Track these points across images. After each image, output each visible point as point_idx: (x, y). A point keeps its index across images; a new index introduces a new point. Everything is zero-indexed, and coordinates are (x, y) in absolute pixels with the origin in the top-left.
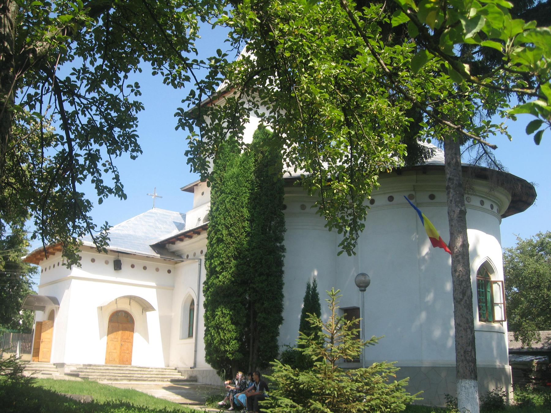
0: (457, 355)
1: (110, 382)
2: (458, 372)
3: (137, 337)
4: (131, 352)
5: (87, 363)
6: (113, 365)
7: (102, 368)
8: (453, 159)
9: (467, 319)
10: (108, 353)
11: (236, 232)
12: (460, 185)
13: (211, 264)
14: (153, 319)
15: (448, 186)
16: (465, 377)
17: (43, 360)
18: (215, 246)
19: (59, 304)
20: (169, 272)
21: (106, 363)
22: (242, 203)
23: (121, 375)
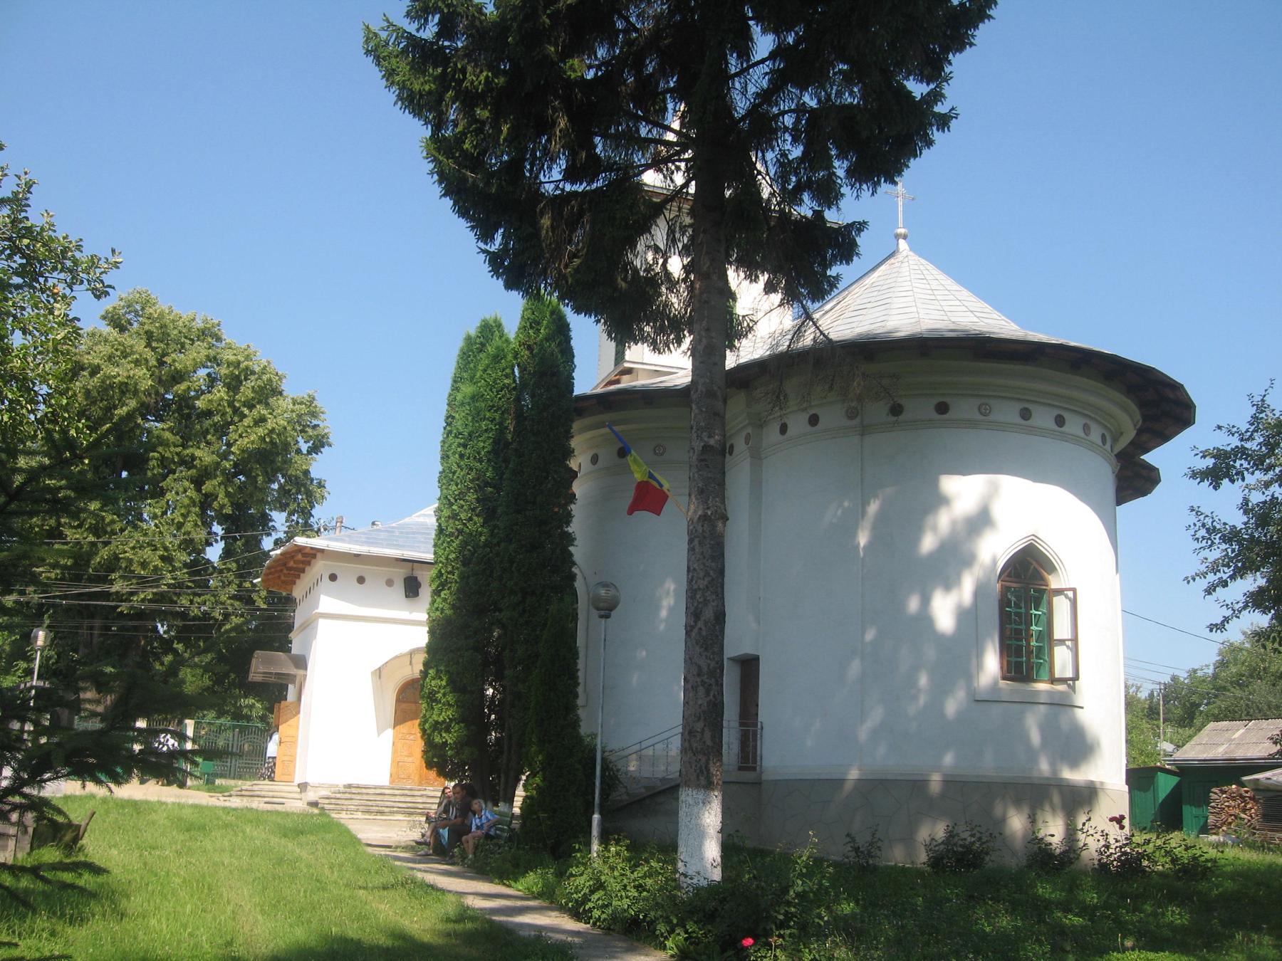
5: (346, 783)
9: (699, 667)
10: (396, 763)
17: (284, 778)
21: (392, 782)
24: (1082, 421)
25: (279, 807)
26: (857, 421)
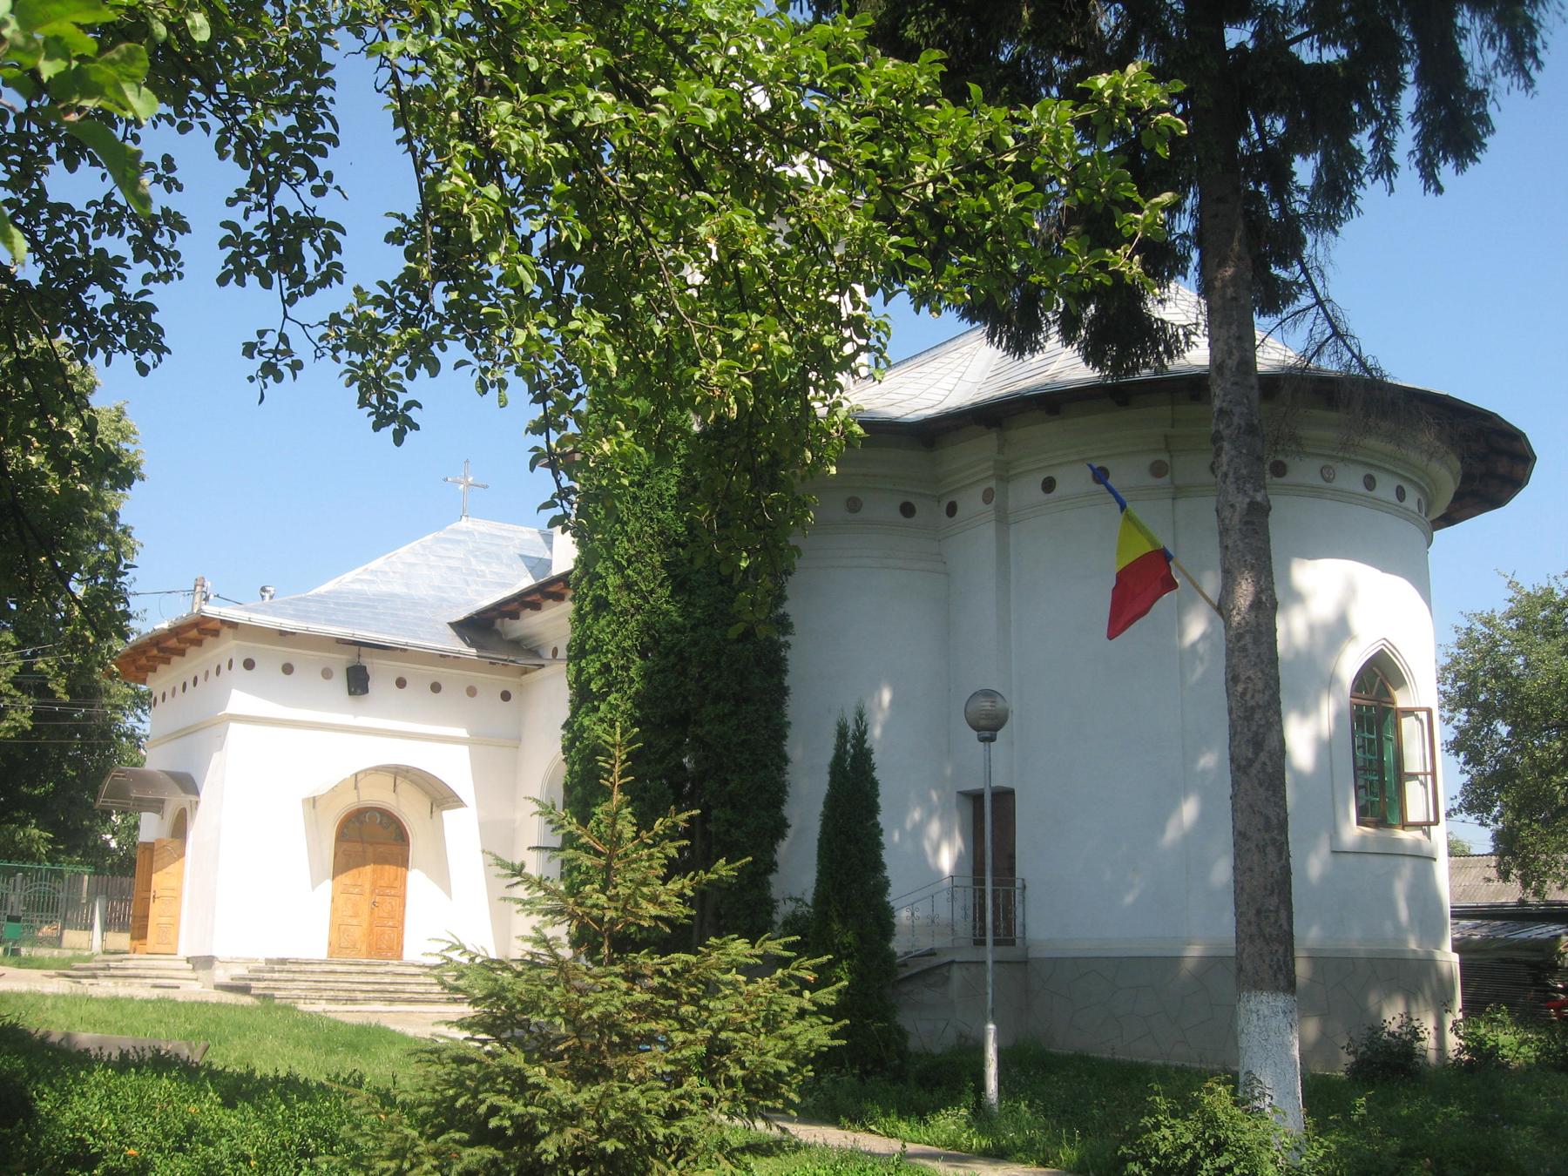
0: (1237, 922)
1: (333, 1007)
2: (1240, 969)
3: (416, 880)
4: (402, 923)
5: (275, 955)
6: (350, 960)
7: (316, 968)
8: (1230, 353)
9: (1267, 819)
10: (337, 927)
11: (644, 579)
12: (1251, 430)
13: (580, 671)
14: (461, 832)
15: (1218, 431)
16: (1257, 985)
18: (589, 620)
19: (197, 794)
20: (506, 696)
21: (331, 954)
22: (661, 496)
23: (369, 987)
25: (171, 993)
26: (1166, 480)
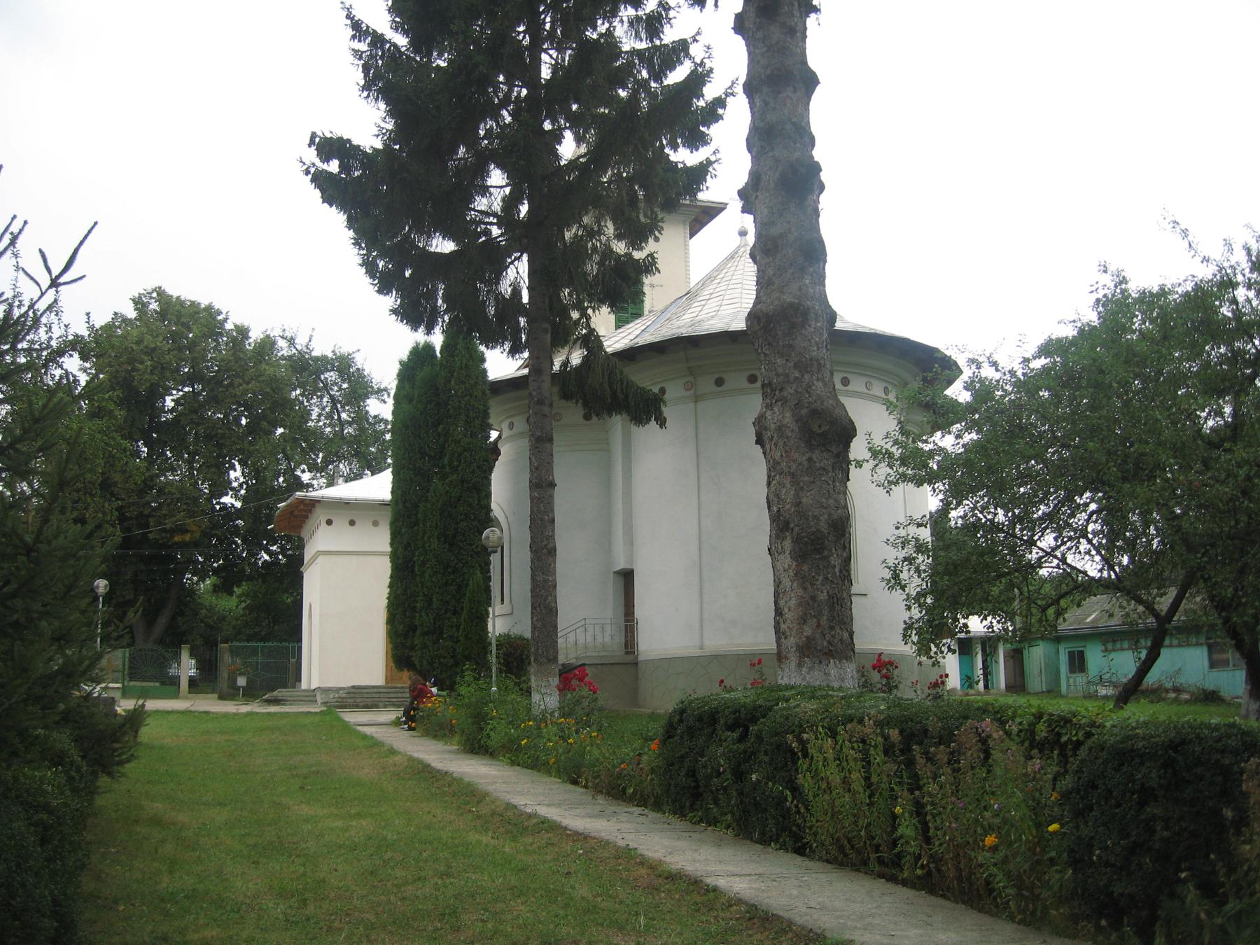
21: (387, 682)
24: (864, 380)
26: (692, 392)
